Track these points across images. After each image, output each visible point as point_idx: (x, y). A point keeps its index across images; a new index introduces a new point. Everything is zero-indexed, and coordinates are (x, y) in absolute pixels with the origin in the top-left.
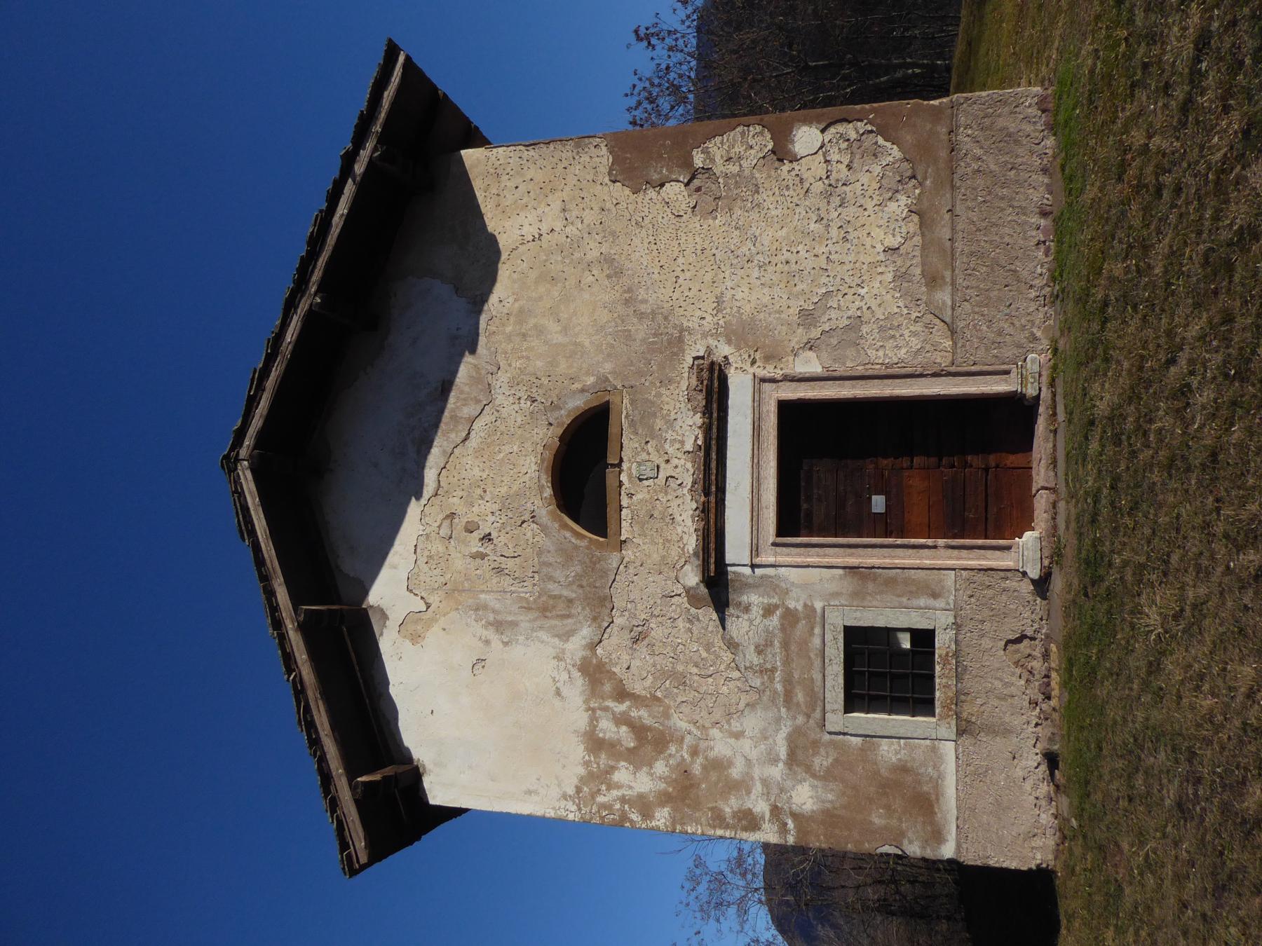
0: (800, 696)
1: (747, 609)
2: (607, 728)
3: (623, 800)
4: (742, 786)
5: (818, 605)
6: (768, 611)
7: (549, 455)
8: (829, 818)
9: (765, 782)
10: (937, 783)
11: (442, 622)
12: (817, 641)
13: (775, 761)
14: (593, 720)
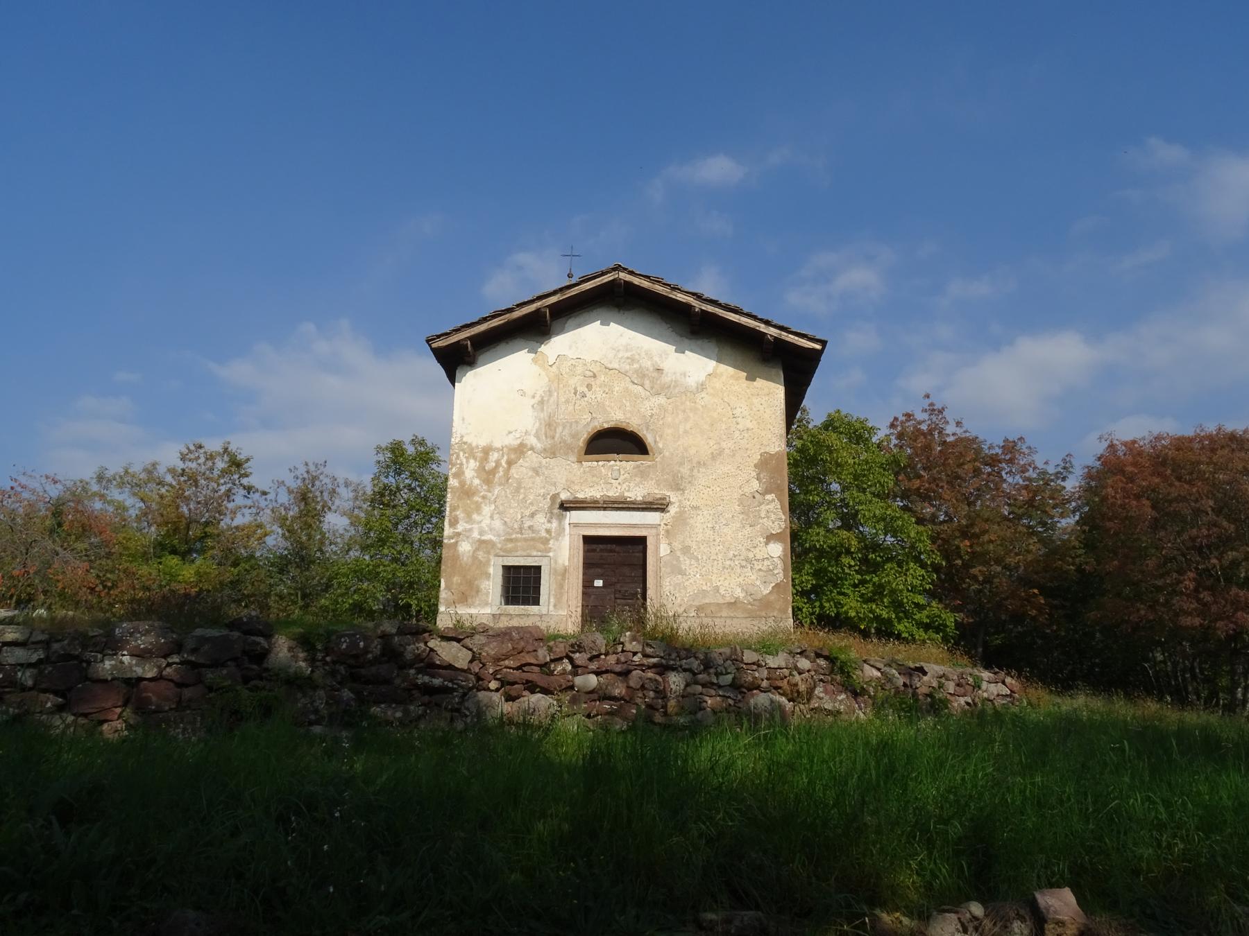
0: (510, 546)
2: (494, 456)
3: (461, 464)
5: (551, 554)
6: (548, 531)
8: (456, 557)
9: (471, 530)
11: (543, 373)
13: (481, 533)
14: (498, 450)
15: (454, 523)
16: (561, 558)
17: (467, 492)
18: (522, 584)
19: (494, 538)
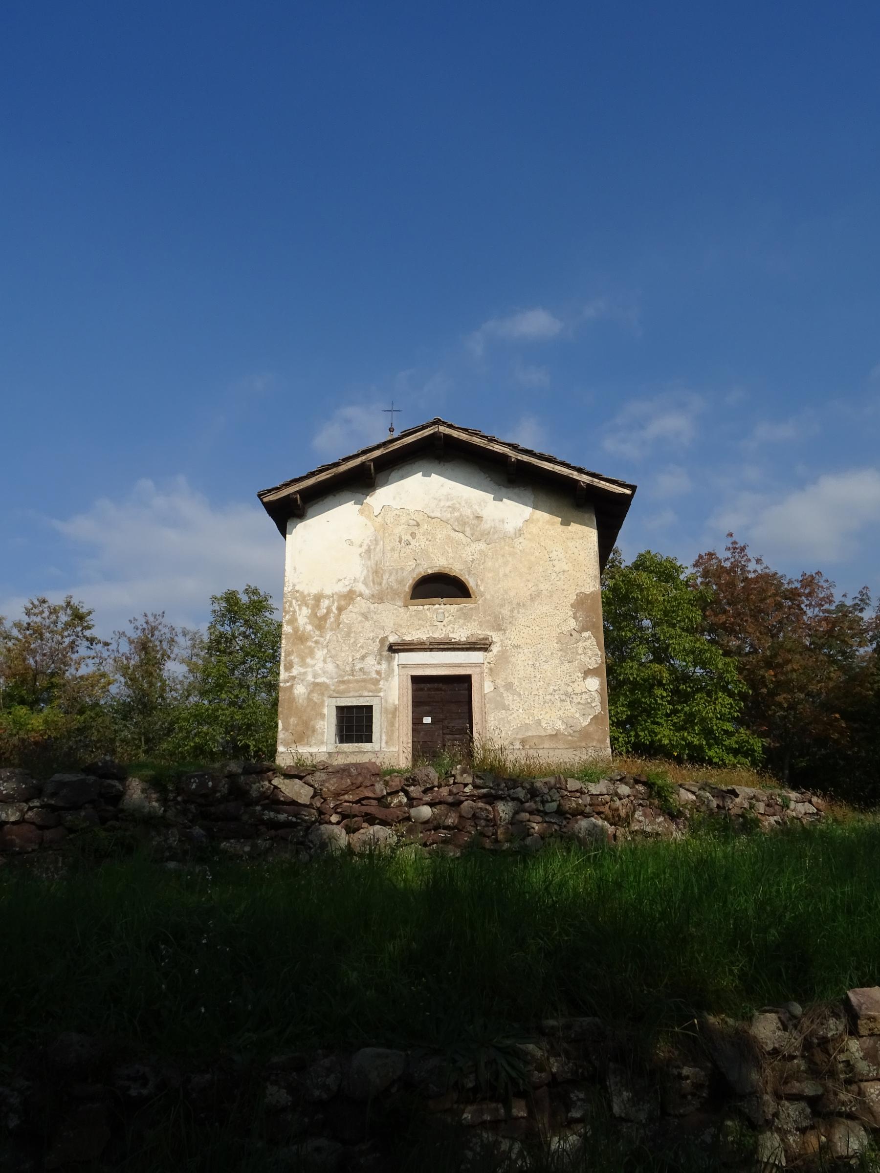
0: (342, 687)
1: (379, 663)
3: (294, 612)
4: (303, 664)
5: (381, 694)
7: (447, 571)
8: (292, 700)
10: (309, 744)
11: (369, 523)
12: (366, 694)
13: (315, 677)
14: (328, 597)
15: (289, 668)
16: (391, 698)
17: (300, 638)
18: (355, 723)
19: (327, 681)
